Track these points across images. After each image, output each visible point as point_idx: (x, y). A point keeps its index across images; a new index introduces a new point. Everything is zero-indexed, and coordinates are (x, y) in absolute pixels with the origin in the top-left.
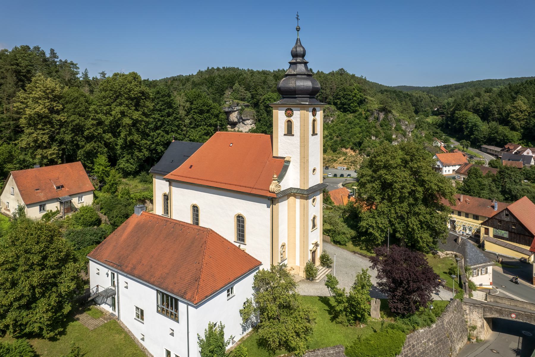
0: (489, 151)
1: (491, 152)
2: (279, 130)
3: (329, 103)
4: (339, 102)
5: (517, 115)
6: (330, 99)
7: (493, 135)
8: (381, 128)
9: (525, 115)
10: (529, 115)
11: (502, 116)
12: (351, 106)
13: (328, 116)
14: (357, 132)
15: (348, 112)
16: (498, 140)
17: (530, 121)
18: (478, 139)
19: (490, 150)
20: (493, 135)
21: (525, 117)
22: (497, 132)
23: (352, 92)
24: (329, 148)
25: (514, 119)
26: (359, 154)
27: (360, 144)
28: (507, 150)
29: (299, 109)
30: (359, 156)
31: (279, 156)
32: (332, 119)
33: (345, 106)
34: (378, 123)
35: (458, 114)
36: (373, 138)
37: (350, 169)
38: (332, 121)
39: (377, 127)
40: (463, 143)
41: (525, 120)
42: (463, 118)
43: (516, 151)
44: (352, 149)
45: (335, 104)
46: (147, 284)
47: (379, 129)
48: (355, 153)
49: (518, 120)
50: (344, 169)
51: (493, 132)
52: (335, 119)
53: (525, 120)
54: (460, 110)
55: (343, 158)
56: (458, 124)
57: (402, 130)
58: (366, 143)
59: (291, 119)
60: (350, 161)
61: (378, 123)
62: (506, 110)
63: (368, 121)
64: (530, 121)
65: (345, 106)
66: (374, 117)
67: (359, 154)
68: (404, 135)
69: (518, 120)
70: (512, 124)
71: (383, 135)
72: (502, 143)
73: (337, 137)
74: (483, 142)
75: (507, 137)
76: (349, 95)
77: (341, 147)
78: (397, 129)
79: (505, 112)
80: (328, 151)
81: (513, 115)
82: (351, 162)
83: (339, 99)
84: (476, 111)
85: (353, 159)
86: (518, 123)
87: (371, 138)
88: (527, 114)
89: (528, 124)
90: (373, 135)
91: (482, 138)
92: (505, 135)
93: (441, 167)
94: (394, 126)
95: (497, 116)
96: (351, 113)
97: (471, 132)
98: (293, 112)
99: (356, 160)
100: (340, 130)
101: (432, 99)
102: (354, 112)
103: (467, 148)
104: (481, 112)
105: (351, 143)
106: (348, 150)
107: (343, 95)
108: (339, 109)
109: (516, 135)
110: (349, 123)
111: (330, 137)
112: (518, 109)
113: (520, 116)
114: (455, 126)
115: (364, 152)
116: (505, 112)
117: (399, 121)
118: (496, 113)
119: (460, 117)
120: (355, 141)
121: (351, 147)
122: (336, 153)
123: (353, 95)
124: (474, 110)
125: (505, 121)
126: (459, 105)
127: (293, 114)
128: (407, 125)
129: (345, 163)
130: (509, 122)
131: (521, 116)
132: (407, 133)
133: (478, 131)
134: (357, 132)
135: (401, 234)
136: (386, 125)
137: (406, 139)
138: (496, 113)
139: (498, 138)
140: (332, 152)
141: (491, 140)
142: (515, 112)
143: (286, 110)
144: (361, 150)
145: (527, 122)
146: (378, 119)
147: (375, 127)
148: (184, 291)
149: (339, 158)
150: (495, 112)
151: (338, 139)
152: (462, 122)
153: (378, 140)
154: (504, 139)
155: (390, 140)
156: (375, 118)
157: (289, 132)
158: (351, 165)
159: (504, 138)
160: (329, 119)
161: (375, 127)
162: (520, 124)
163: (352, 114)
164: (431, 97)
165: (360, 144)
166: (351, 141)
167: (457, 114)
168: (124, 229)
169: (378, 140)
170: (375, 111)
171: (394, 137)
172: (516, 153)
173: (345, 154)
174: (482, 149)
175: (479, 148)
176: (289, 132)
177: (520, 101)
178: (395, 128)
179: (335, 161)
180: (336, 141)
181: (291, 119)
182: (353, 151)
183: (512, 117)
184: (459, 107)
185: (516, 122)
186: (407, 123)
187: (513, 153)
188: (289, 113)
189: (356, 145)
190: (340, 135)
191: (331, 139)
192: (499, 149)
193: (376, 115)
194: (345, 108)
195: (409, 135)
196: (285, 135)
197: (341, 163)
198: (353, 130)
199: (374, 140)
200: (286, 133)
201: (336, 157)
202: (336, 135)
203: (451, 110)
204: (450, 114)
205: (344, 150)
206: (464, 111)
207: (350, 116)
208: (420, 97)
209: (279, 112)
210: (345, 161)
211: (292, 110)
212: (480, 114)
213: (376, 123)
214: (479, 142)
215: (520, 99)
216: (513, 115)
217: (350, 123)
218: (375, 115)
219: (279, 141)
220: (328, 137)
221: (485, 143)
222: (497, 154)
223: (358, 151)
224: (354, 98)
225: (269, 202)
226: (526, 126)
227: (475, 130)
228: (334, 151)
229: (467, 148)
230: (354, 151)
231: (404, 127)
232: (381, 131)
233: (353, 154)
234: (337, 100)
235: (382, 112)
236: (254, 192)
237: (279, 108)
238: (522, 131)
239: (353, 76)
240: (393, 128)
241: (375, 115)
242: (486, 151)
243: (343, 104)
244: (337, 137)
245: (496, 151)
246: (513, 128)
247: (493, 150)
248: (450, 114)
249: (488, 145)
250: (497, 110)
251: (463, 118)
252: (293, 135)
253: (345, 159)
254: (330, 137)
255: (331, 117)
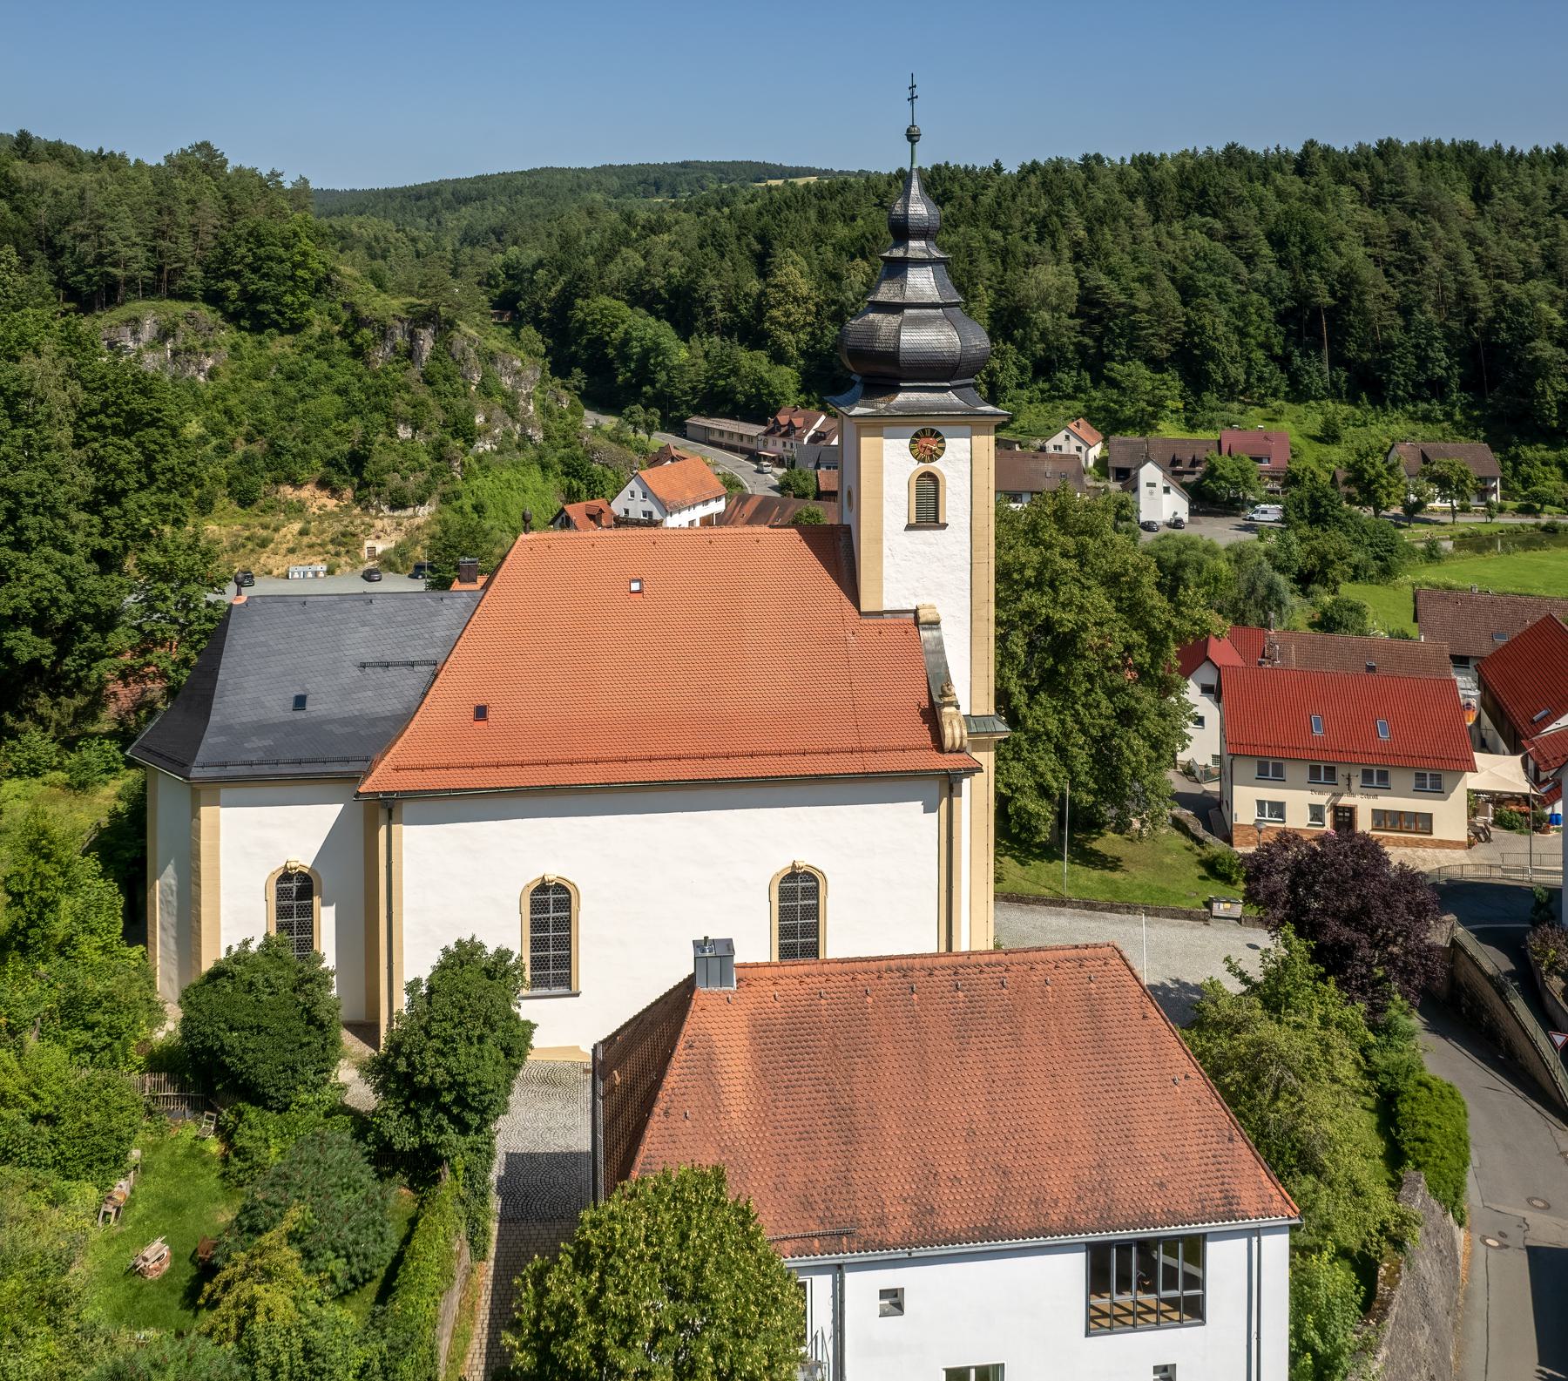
0: (715, 437)
1: (725, 440)
2: (886, 511)
3: (185, 296)
4: (233, 288)
5: (788, 314)
6: (191, 278)
7: (722, 383)
8: (429, 390)
9: (809, 312)
10: (818, 313)
11: (740, 316)
12: (287, 305)
13: (189, 350)
14: (330, 414)
15: (273, 330)
16: (740, 398)
17: (822, 329)
18: (672, 396)
19: (722, 432)
20: (722, 383)
21: (809, 319)
22: (735, 372)
23: (287, 247)
24: (222, 491)
25: (780, 324)
26: (358, 501)
27: (357, 461)
28: (783, 430)
29: (968, 429)
30: (357, 511)
31: (887, 606)
32: (209, 363)
33: (262, 307)
34: (415, 372)
35: (583, 308)
36: (404, 432)
37: (338, 572)
38: (212, 374)
39: (414, 387)
40: (637, 418)
41: (809, 329)
42: (605, 325)
43: (812, 432)
44: (323, 484)
45: (214, 299)
46: (1042, 1241)
47: (423, 393)
48: (340, 498)
49: (790, 329)
50: (316, 574)
51: (721, 371)
52: (224, 364)
53: (809, 329)
54: (587, 297)
55: (297, 526)
56: (586, 348)
57: (504, 394)
58: (381, 457)
59: (937, 466)
60: (327, 537)
61: (415, 372)
62: (747, 294)
63: (367, 364)
64: (822, 329)
65: (262, 307)
66: (394, 349)
67: (358, 501)
68: (512, 411)
69: (789, 327)
70: (775, 343)
71: (440, 415)
72: (759, 408)
73: (250, 439)
74: (689, 407)
75: (768, 385)
76: (281, 261)
77: (276, 482)
78: (486, 391)
79: (747, 302)
80: (218, 505)
81: (775, 313)
82: (332, 541)
83: (237, 276)
84: (639, 297)
85: (338, 527)
86: (791, 337)
87: (393, 434)
88: (813, 309)
89: (819, 342)
90: (405, 421)
91: (685, 393)
92: (761, 379)
93: (657, 516)
94: (477, 378)
95: (721, 315)
96: (283, 332)
97: (644, 374)
98: (943, 441)
99: (350, 529)
100: (255, 408)
101: (421, 246)
102: (296, 328)
103: (649, 433)
104: (663, 301)
105: (317, 464)
106: (306, 493)
107: (249, 260)
108: (233, 318)
109: (785, 378)
110: (289, 378)
111: (214, 442)
112: (788, 294)
113: (797, 316)
114: (576, 352)
115: (378, 495)
116: (747, 302)
117: (491, 358)
118: (718, 307)
119: (594, 322)
120: (330, 454)
121: (317, 475)
122: (255, 509)
123: (298, 258)
124: (630, 292)
125: (752, 332)
126: (581, 278)
127: (943, 449)
128: (518, 372)
129: (311, 546)
130: (766, 335)
131: (798, 313)
132: (522, 403)
133: (668, 369)
134: (330, 414)
135: (1089, 792)
136: (447, 378)
137: (518, 427)
138: (718, 307)
139: (740, 392)
140: (235, 507)
141: (717, 401)
142: (779, 303)
143: (916, 435)
144: (364, 485)
145: (812, 334)
146: (410, 354)
147: (407, 389)
148: (1218, 1195)
149: (276, 530)
150: (714, 302)
151: (255, 448)
152: (600, 338)
153: (421, 441)
154: (759, 394)
155: (468, 435)
156: (397, 353)
157: (928, 514)
158: (338, 554)
159: (758, 389)
160: (200, 363)
161: (407, 389)
162: (797, 343)
163: (289, 338)
164: (414, 240)
165: (357, 461)
166: (315, 450)
167: (582, 310)
168: (708, 1066)
169: (421, 441)
170: (398, 324)
171: (479, 420)
172: (814, 439)
173: (298, 509)
174: (689, 429)
175: (679, 428)
176: (928, 514)
177: (791, 268)
178: (482, 385)
179: (263, 544)
180: (247, 460)
181: (937, 466)
182: (327, 493)
183: (773, 320)
184: (582, 285)
185: (786, 338)
186: (518, 363)
187: (806, 440)
188: (927, 441)
189: (341, 470)
190: (260, 432)
191: (222, 450)
192: (755, 430)
193: (400, 339)
194: (264, 314)
195: (527, 410)
196: (909, 527)
197: (292, 551)
198: (311, 404)
199: (407, 440)
200: (913, 521)
201: (265, 527)
202: (242, 429)
203: (552, 294)
204: (550, 310)
205: (287, 491)
206: (604, 301)
207: (280, 346)
208: (377, 239)
209: (887, 443)
210: (306, 540)
211: (938, 435)
212: (660, 307)
213: (407, 373)
214: (677, 408)
215: (789, 260)
216: (775, 313)
217: (290, 377)
218: (399, 339)
219: (886, 551)
220: (206, 442)
221: (697, 411)
222: (752, 446)
223: (348, 493)
224: (300, 273)
225: (934, 787)
226: (813, 347)
227: (657, 364)
228: (245, 500)
229: (649, 433)
230: (335, 492)
231: (507, 382)
232: (431, 402)
233: (331, 504)
234: (228, 283)
235: (425, 327)
236: (876, 763)
237: (886, 430)
238: (802, 362)
239: (302, 186)
240: (473, 388)
241: (399, 339)
242: (705, 438)
243: (251, 298)
244: (250, 439)
245: (741, 436)
246: (779, 357)
247: (731, 434)
248: (550, 310)
249: (709, 416)
250: (720, 297)
251: (605, 325)
252: (944, 526)
253: (303, 532)
254: (214, 442)
255: (208, 355)
